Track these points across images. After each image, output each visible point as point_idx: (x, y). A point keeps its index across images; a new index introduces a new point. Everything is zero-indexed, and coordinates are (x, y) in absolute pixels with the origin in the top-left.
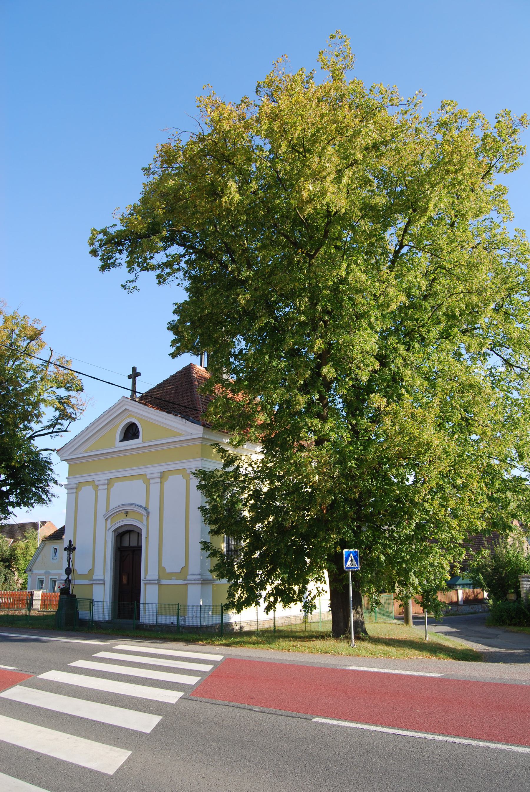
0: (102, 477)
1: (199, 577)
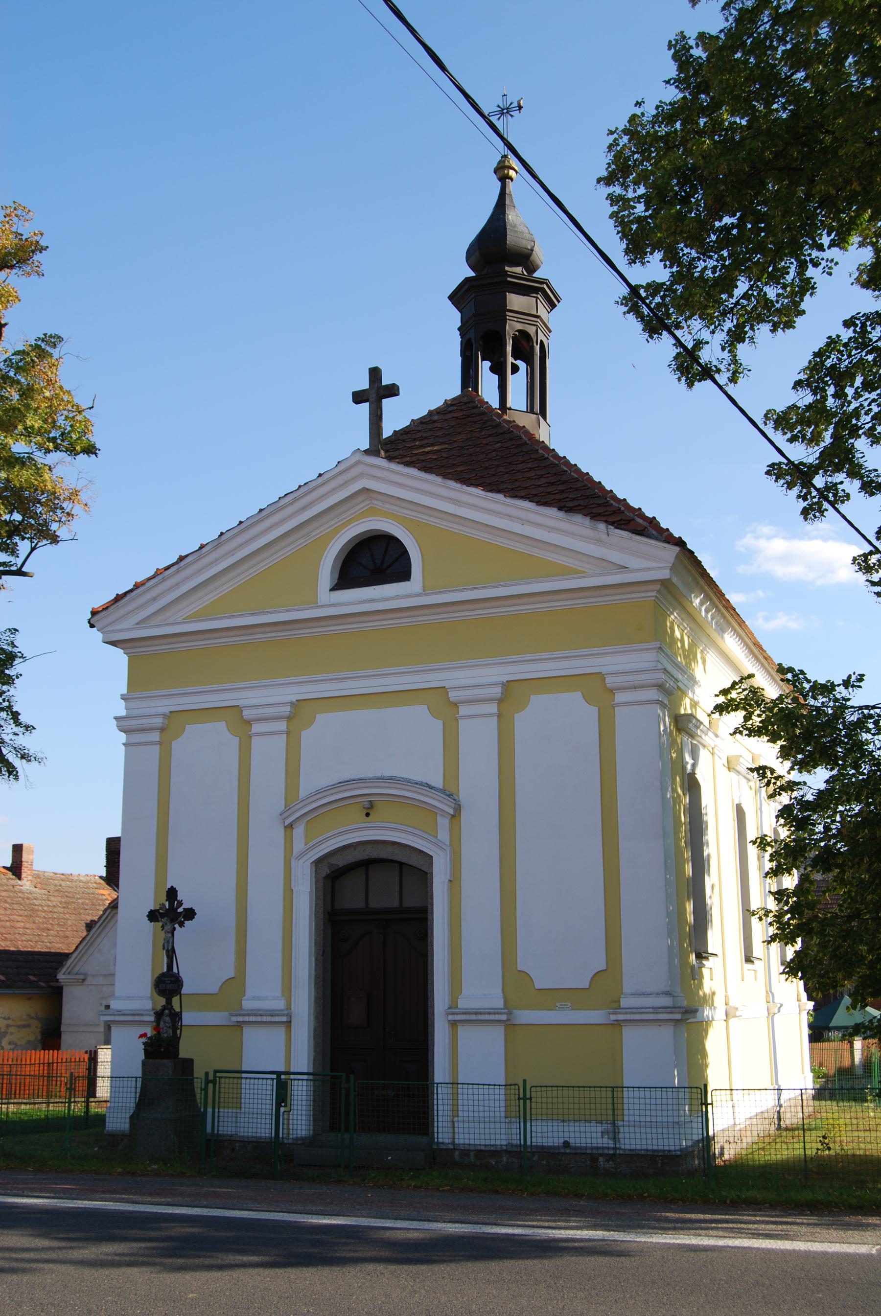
0: (281, 694)
1: (666, 1001)
